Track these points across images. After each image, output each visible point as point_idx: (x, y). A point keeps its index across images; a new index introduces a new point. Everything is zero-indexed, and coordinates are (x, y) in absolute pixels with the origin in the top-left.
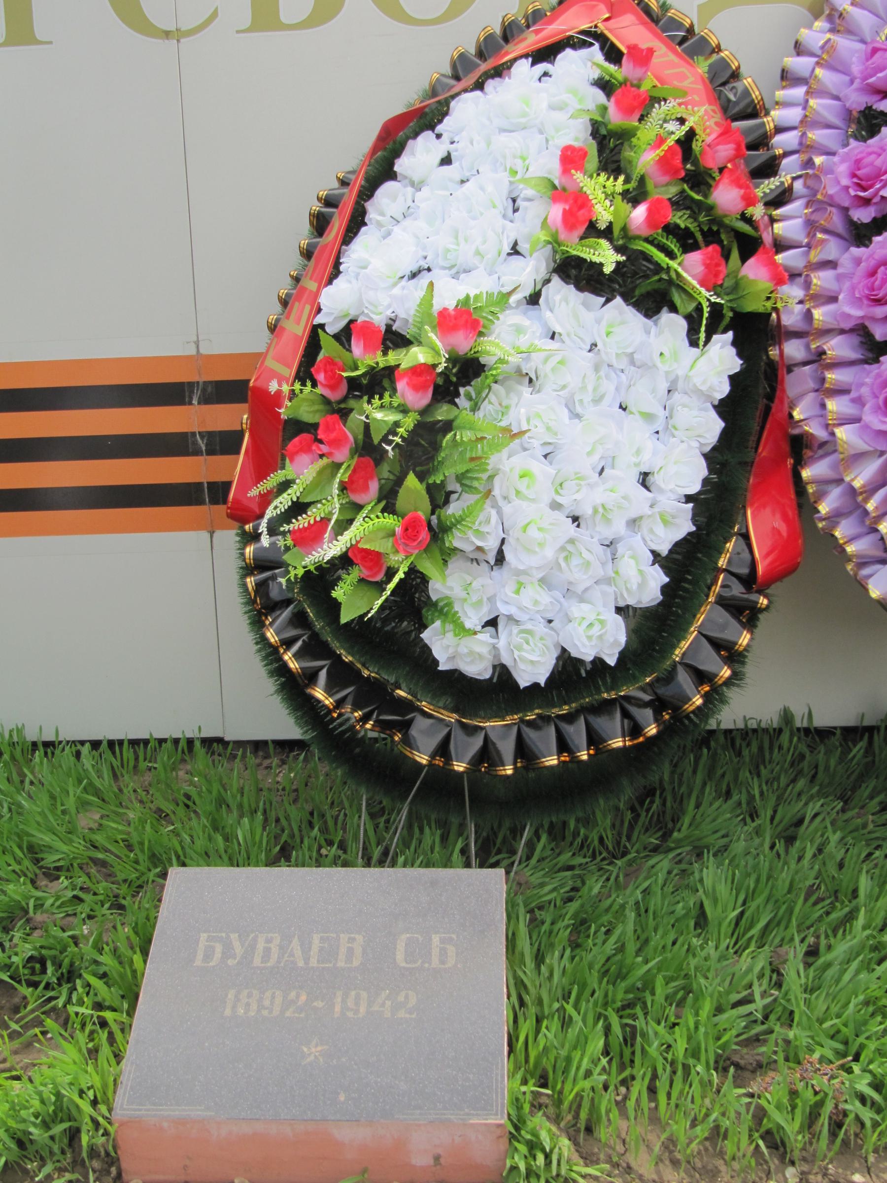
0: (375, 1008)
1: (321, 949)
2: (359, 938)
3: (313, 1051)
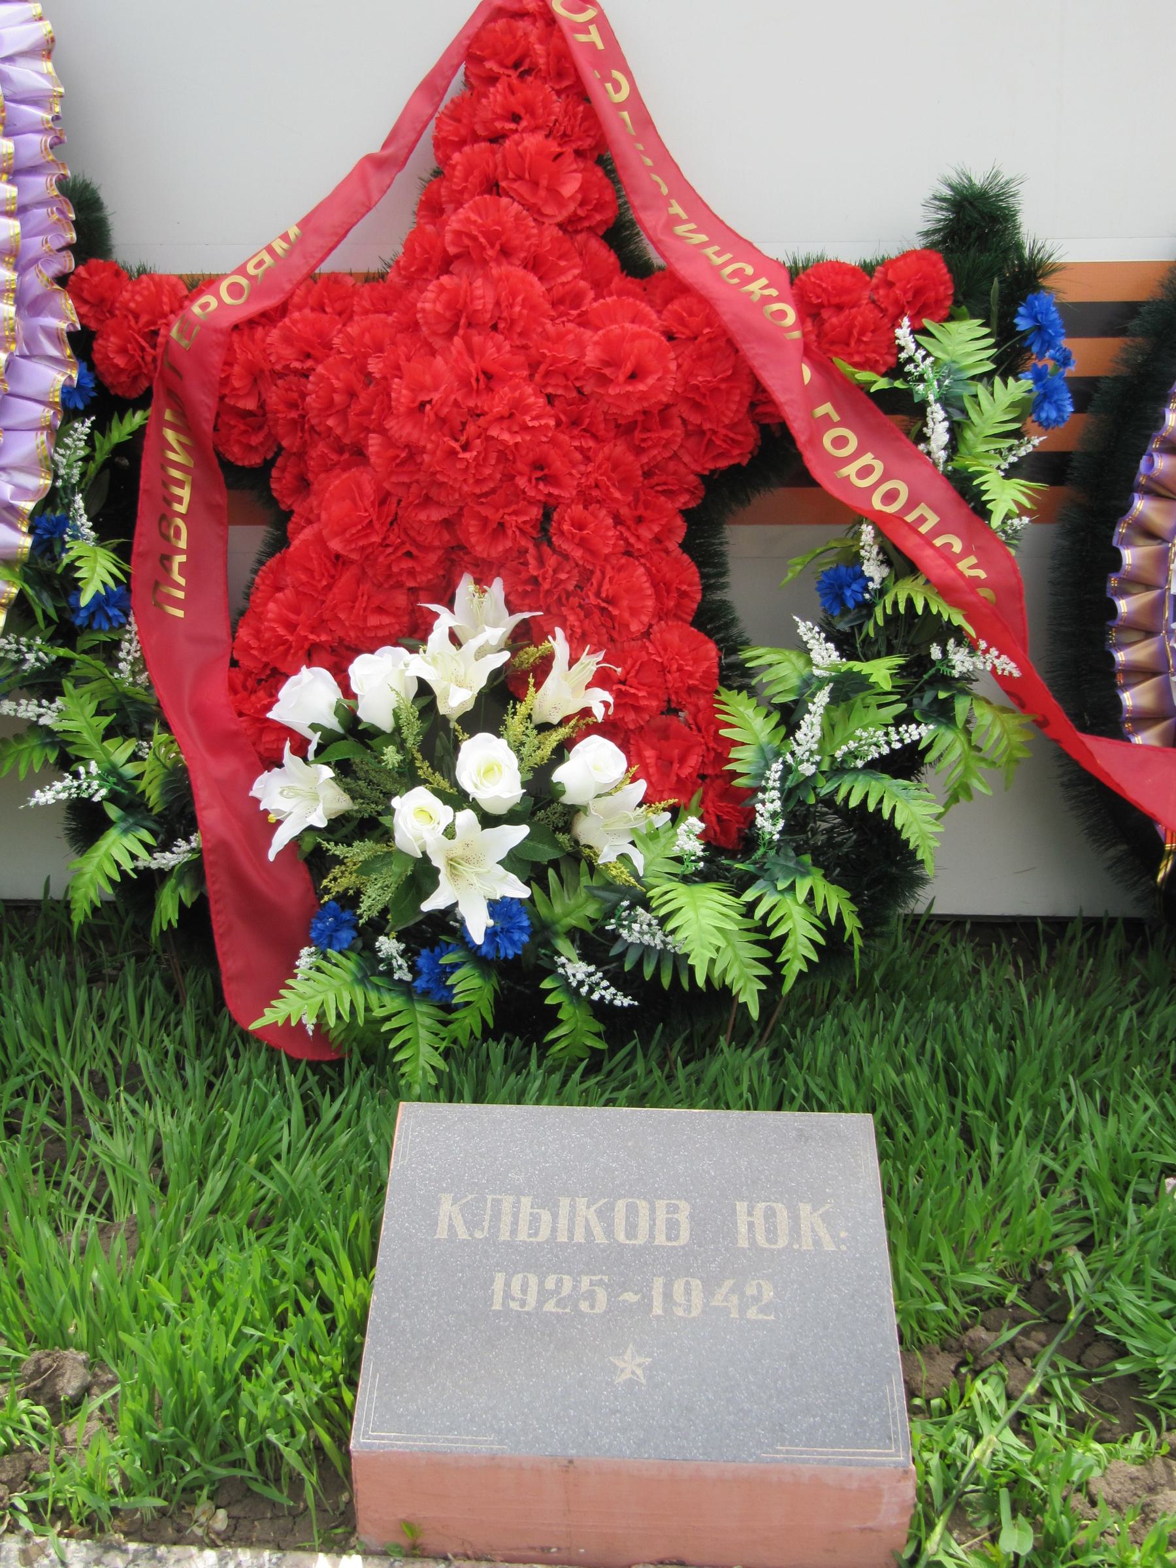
2: (685, 1207)
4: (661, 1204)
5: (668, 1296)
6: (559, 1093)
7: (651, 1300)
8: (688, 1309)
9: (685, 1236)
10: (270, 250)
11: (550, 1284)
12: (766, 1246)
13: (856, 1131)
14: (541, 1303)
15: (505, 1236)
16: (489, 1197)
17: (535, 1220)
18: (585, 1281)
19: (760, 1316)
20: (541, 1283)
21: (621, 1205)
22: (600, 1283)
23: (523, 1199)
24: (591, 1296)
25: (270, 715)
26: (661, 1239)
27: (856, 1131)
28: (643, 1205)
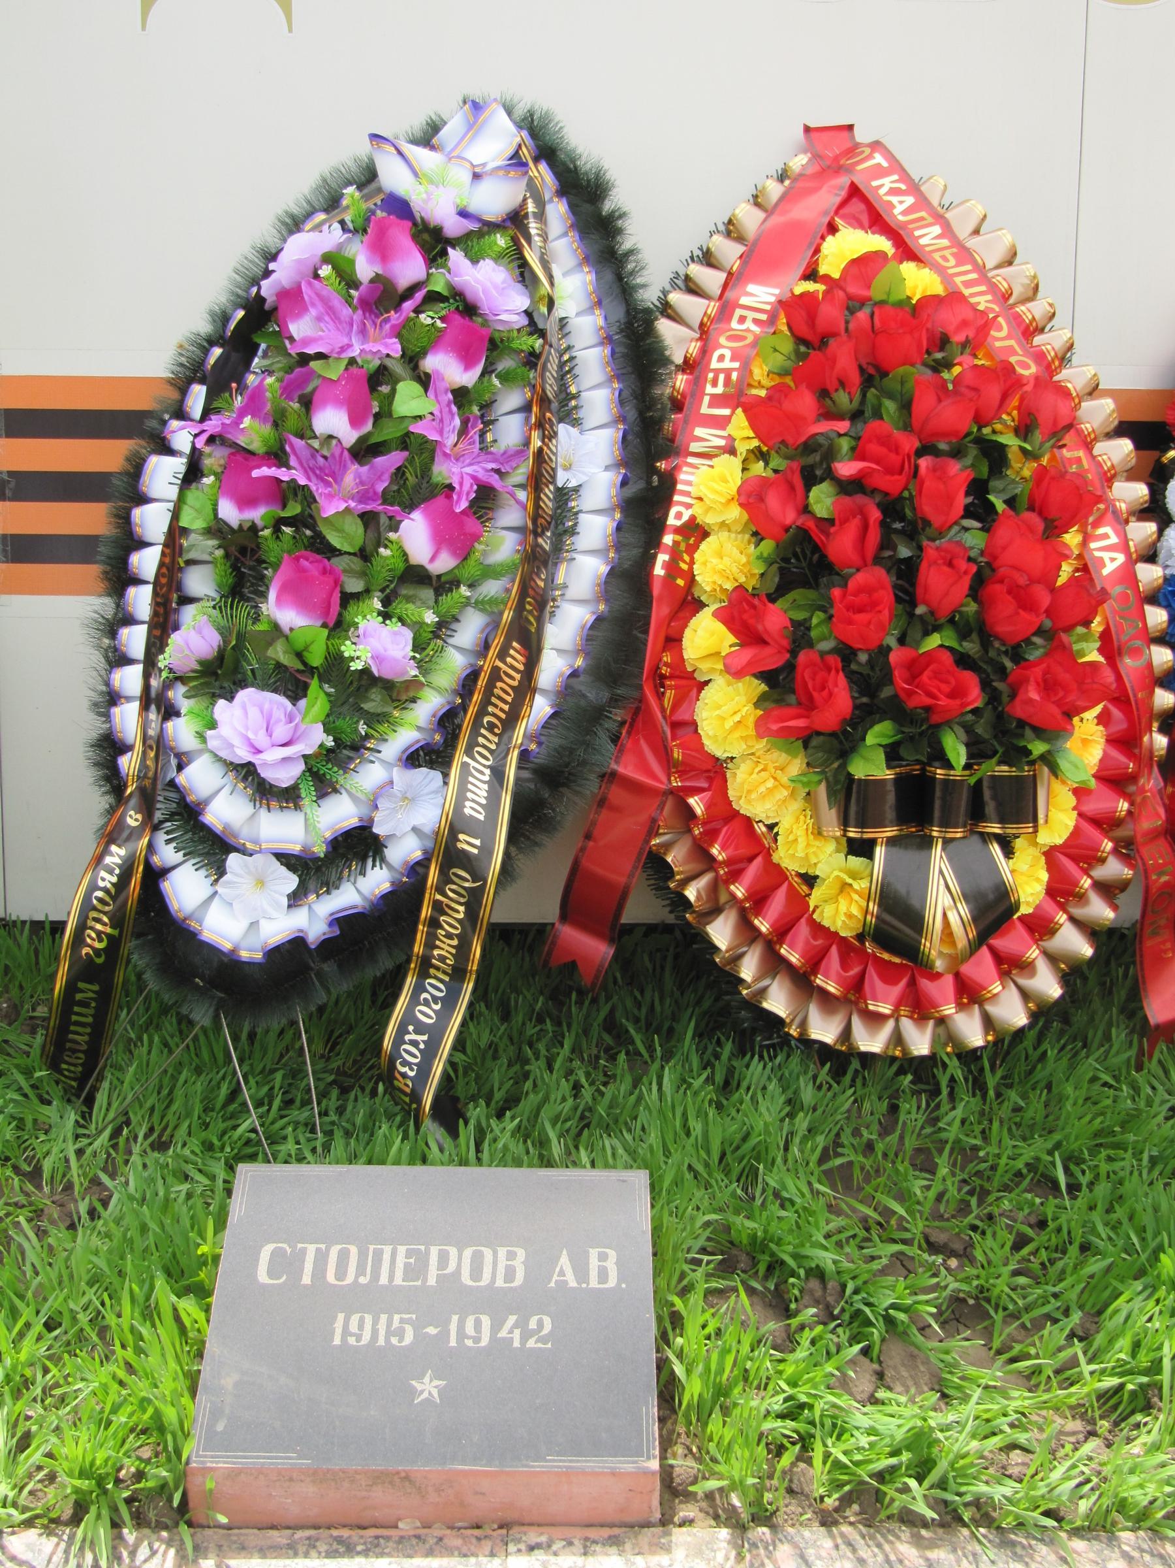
0: (503, 1334)
1: (407, 1265)
2: (521, 1254)
4: (502, 1252)
5: (375, 1332)
6: (479, 1159)
7: (448, 1332)
9: (519, 1280)
10: (731, 230)
11: (533, 1324)
12: (470, 1283)
13: (640, 1179)
15: (384, 1280)
16: (372, 1247)
18: (396, 1317)
19: (540, 1345)
21: (311, 1249)
22: (408, 1321)
24: (400, 1333)
25: (623, 921)
26: (500, 1283)
27: (640, 1179)
28: (488, 1253)
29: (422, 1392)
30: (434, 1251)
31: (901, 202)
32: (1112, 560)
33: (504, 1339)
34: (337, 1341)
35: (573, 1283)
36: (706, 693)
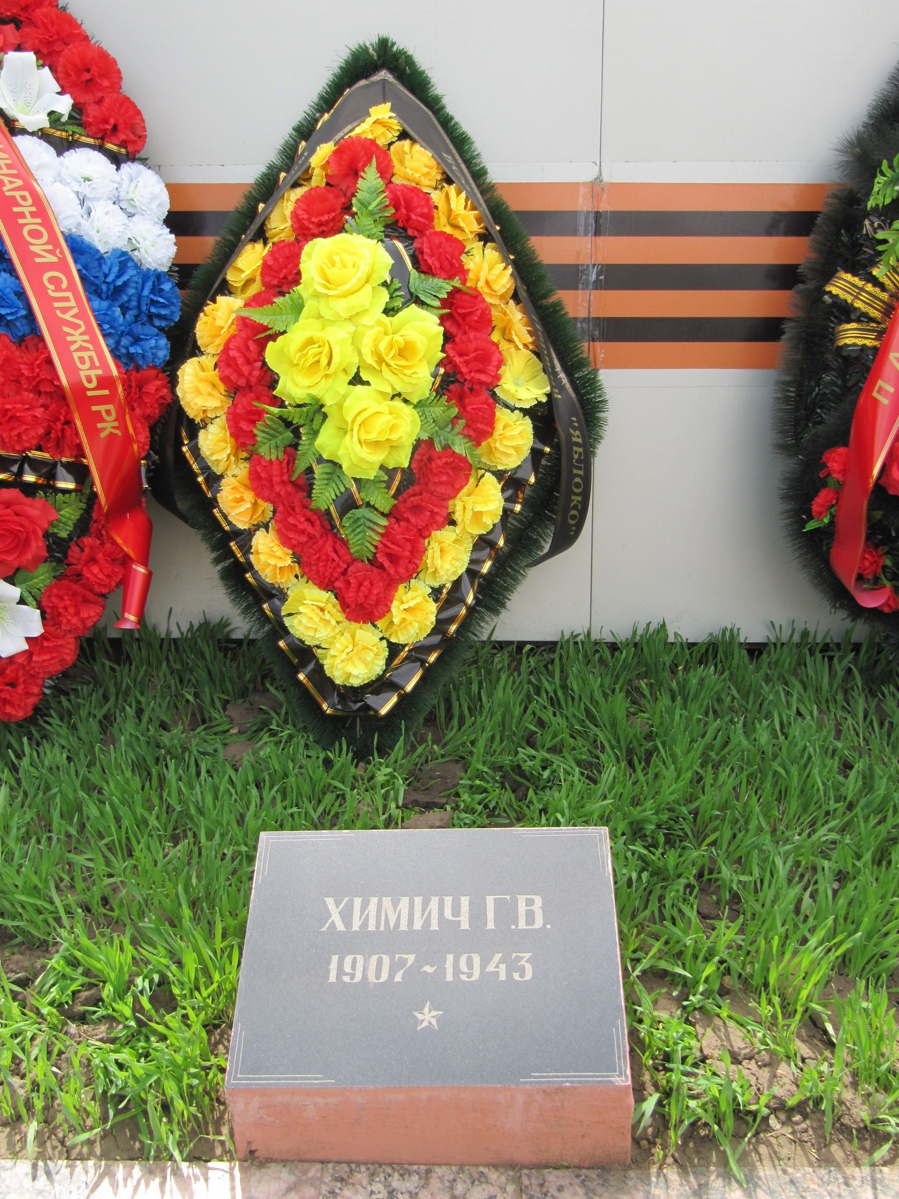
0: (490, 968)
2: (538, 900)
3: (428, 1017)
8: (470, 975)
14: (391, 976)
17: (456, 911)
20: (392, 959)
23: (384, 899)
29: (430, 1022)
30: (522, 900)
31: (11, 182)
32: (11, 182)
33: (490, 973)
34: (333, 978)
35: (340, 927)
36: (223, 482)
